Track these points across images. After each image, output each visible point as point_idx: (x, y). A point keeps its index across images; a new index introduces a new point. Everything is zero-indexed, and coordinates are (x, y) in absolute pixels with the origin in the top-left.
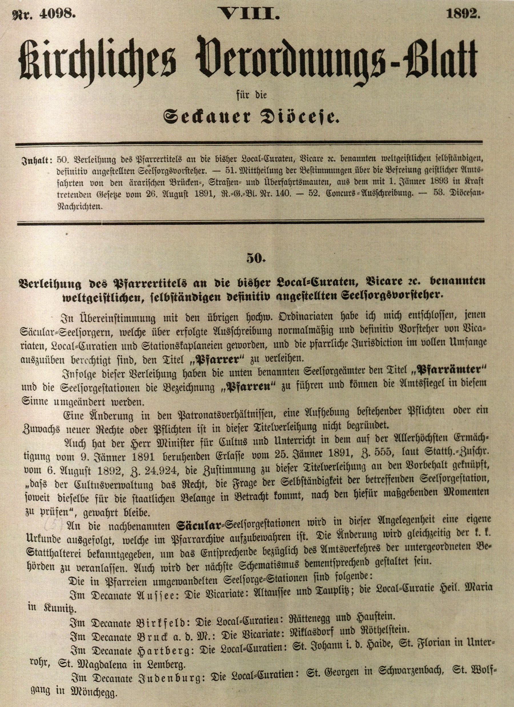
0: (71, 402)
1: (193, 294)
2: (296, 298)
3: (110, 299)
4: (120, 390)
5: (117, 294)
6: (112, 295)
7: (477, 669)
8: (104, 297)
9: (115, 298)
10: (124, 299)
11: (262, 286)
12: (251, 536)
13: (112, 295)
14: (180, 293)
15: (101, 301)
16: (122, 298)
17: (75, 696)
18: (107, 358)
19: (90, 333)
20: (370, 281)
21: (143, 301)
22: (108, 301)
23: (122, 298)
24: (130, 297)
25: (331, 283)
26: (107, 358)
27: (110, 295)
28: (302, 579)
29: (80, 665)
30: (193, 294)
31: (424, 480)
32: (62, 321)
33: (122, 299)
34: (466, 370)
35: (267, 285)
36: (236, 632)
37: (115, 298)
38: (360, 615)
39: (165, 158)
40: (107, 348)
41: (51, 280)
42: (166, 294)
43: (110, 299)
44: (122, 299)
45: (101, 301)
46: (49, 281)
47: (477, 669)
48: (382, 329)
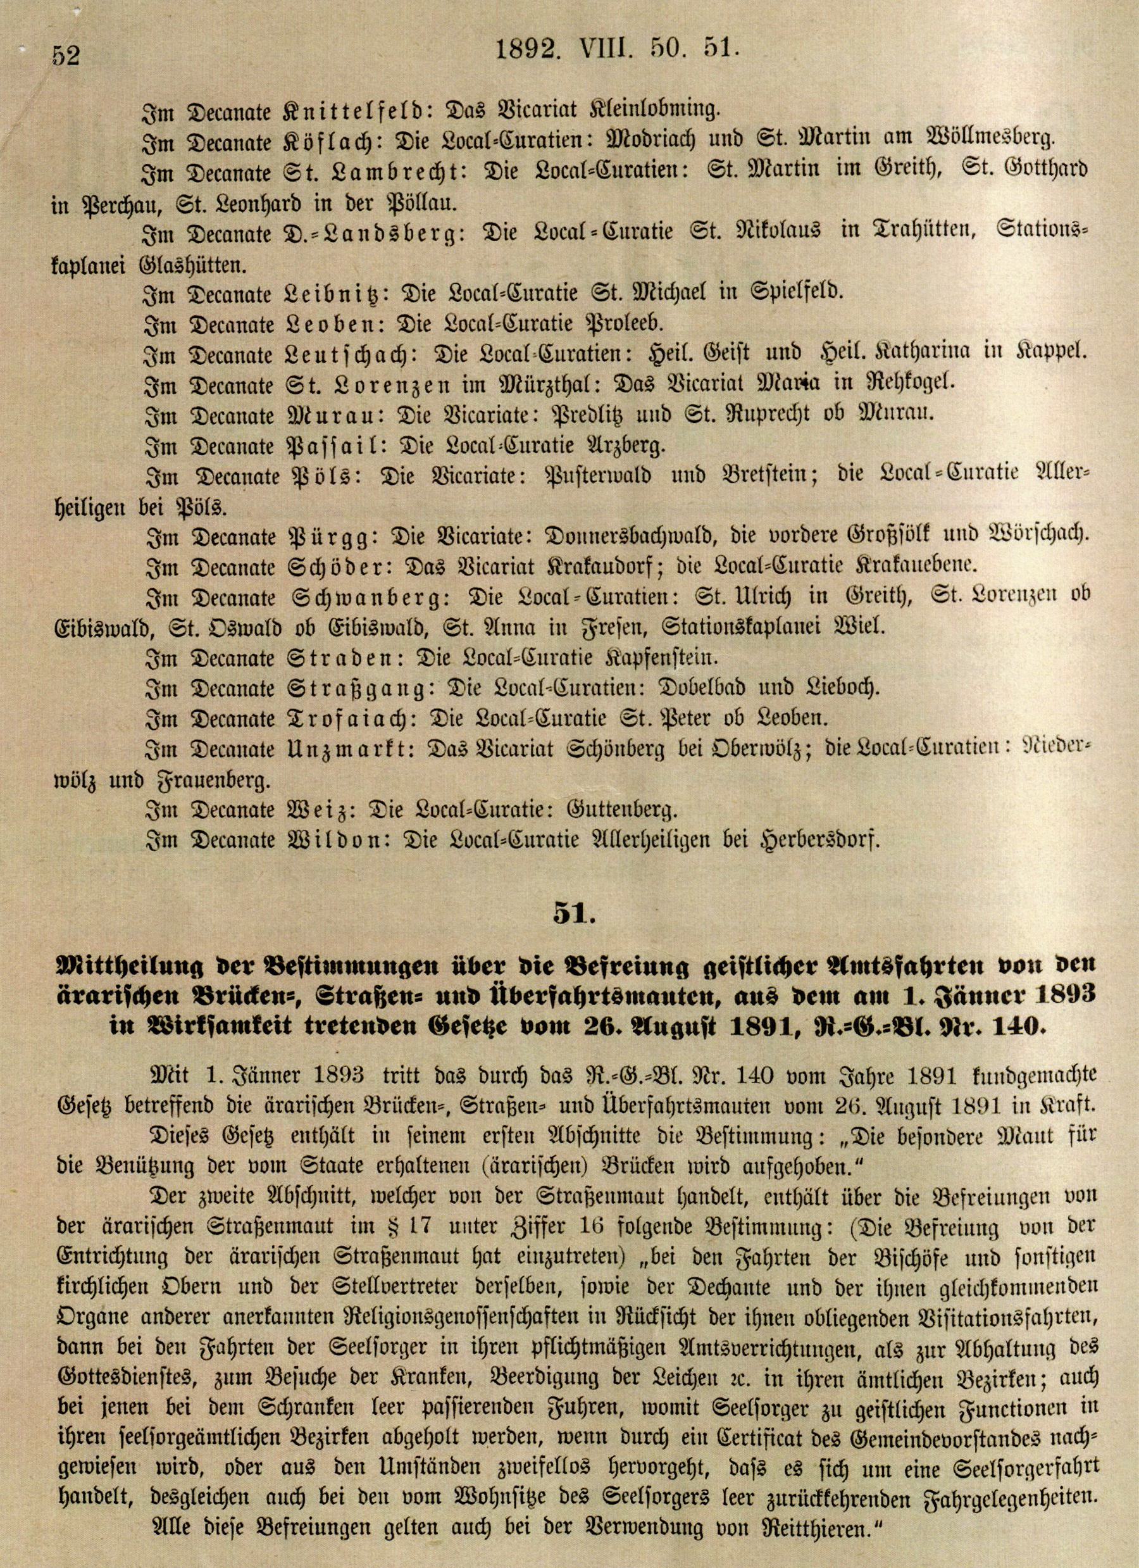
0: (684, 839)
1: (469, 990)
2: (717, 970)
3: (753, 968)
4: (712, 630)
5: (767, 957)
6: (758, 960)
7: (468, 1495)
8: (742, 964)
9: (763, 968)
10: (142, 997)
11: (799, 973)
12: (573, 1403)
13: (758, 960)
14: (957, 987)
15: (734, 972)
16: (250, 997)
17: (765, 393)
18: (569, 104)
19: (1023, 1471)
20: (836, 965)
21: (798, 1034)
22: (308, 972)
23: (250, 997)
24: (796, 965)
25: (83, 998)
26: (569, 104)
27: (753, 960)
28: (605, 1259)
29: (762, 386)
30: (469, 990)
31: (939, 598)
32: (148, 664)
33: (138, 998)
34: (677, 998)
35: (811, 972)
36: (627, 1279)
37: (763, 968)
38: (487, 1533)
39: (848, 133)
40: (563, 327)
41: (733, 957)
42: (472, 959)
43: (753, 968)
44: (138, 998)
45: (734, 972)
46: (729, 960)
47: (468, 1495)
48: (336, 1196)
